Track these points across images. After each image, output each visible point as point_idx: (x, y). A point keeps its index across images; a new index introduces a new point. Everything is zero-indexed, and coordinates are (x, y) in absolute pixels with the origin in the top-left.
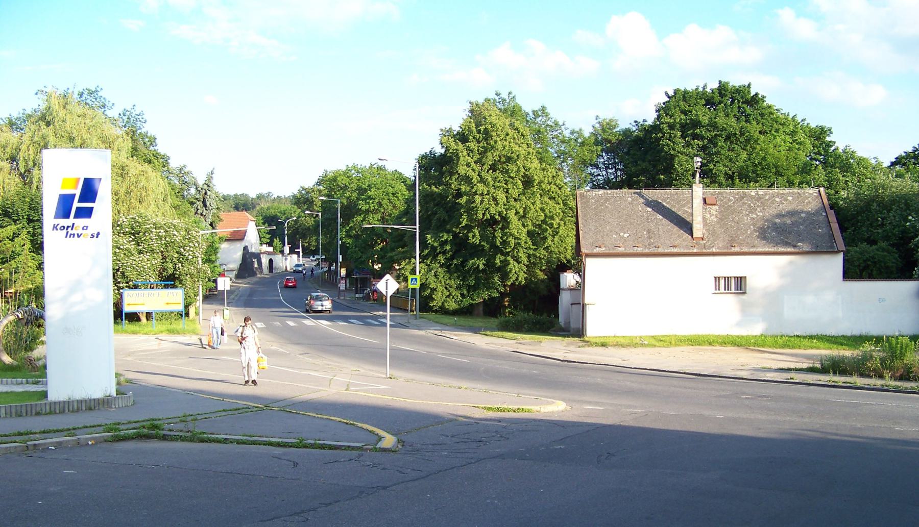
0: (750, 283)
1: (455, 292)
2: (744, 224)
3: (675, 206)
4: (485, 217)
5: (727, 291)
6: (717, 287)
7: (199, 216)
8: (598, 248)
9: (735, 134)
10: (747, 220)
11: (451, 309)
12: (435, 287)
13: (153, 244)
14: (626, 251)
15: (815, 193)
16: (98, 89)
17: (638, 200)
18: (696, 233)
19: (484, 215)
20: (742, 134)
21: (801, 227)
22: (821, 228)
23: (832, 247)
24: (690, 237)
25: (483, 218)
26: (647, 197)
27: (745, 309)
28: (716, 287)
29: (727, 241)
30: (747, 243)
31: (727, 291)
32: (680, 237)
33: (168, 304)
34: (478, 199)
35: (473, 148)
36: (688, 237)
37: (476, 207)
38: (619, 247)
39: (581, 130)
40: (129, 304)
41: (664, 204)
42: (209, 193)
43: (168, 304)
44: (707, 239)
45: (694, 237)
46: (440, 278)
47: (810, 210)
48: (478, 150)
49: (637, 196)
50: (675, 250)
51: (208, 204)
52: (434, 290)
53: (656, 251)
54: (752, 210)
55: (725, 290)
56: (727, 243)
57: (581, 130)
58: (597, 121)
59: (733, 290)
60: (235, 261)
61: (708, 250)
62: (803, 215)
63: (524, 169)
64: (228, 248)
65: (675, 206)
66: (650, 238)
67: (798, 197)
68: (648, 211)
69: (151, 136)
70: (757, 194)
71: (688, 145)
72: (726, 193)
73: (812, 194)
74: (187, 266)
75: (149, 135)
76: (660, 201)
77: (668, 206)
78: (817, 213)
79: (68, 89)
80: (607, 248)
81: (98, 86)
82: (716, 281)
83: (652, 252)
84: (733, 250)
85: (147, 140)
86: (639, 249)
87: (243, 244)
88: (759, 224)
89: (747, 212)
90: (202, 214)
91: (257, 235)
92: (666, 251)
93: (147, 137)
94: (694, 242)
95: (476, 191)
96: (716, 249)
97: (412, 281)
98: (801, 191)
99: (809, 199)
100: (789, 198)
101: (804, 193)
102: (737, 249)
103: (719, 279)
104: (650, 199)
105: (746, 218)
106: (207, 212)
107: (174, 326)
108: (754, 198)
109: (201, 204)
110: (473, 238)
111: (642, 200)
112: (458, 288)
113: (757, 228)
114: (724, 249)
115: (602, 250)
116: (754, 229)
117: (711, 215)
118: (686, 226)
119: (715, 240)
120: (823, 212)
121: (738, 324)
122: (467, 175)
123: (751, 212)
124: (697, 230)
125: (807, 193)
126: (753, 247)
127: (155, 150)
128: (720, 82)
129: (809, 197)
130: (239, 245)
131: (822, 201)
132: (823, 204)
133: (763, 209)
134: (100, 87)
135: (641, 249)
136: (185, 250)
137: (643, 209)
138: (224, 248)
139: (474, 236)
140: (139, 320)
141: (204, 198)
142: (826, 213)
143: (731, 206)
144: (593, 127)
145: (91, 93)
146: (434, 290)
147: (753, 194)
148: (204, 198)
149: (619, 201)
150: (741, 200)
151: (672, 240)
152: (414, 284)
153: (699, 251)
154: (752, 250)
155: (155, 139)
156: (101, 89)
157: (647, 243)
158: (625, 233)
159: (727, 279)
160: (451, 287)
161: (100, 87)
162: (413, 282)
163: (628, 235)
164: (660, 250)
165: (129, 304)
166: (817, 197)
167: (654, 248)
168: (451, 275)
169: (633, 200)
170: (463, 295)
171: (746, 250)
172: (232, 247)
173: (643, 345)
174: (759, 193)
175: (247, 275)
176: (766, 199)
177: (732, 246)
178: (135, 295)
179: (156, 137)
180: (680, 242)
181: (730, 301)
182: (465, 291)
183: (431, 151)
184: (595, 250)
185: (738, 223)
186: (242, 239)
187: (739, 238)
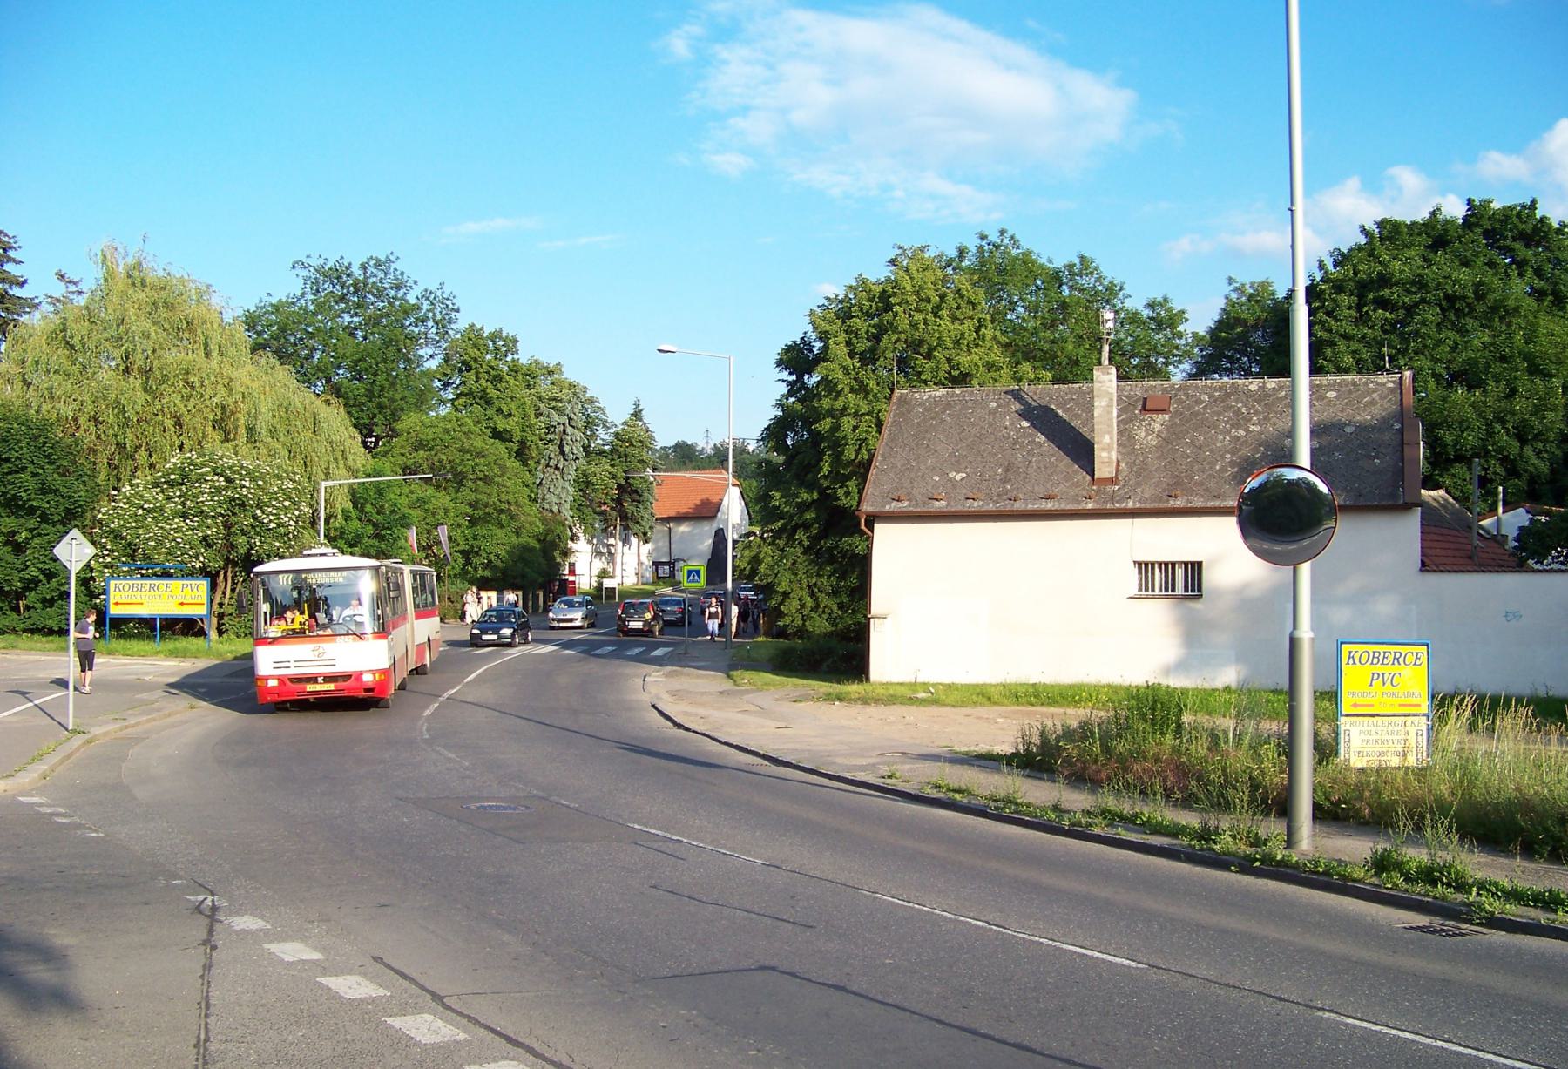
0: (1210, 578)
1: (825, 601)
2: (1212, 451)
3: (1081, 415)
4: (860, 456)
5: (1143, 593)
6: (1146, 585)
7: (552, 470)
8: (894, 504)
9: (1464, 298)
10: (1223, 441)
11: (818, 632)
12: (788, 590)
13: (202, 502)
14: (949, 509)
15: (1391, 382)
16: (392, 258)
17: (1008, 405)
18: (1100, 469)
19: (858, 451)
20: (1480, 297)
21: (1337, 454)
22: (1381, 455)
23: (1394, 496)
24: (1089, 478)
25: (856, 457)
26: (1030, 400)
27: (1193, 634)
28: (1140, 585)
29: (1164, 486)
30: (1207, 490)
31: (1143, 593)
32: (1068, 477)
33: (182, 604)
34: (847, 423)
35: (857, 329)
36: (1084, 478)
37: (844, 438)
38: (937, 500)
39: (1165, 299)
40: (117, 604)
41: (1060, 412)
42: (569, 430)
43: (182, 604)
44: (1122, 483)
45: (1096, 477)
46: (800, 575)
47: (1369, 418)
48: (867, 333)
49: (1010, 397)
50: (1049, 505)
51: (566, 449)
52: (786, 595)
53: (1009, 508)
54: (1240, 421)
55: (1186, 590)
56: (1164, 490)
57: (1165, 299)
58: (1231, 288)
59: (1180, 590)
60: (699, 556)
61: (1117, 505)
62: (1348, 430)
63: (949, 363)
64: (689, 532)
65: (1081, 415)
66: (1004, 481)
67: (1350, 392)
68: (1022, 428)
69: (507, 337)
70: (1263, 388)
71: (1363, 319)
72: (1197, 387)
73: (1384, 384)
74: (269, 540)
75: (504, 335)
76: (1053, 407)
77: (1065, 416)
78: (1384, 424)
79: (342, 257)
80: (914, 502)
81: (392, 253)
82: (1140, 572)
83: (1002, 509)
84: (1172, 503)
85: (501, 343)
86: (976, 504)
87: (715, 526)
88: (1246, 451)
89: (1228, 426)
90: (557, 468)
91: (742, 511)
92: (1030, 507)
93: (501, 338)
94: (1095, 487)
95: (845, 409)
96: (1134, 502)
97: (689, 577)
98: (1360, 379)
99: (1374, 395)
100: (1331, 395)
101: (1366, 384)
102: (1179, 503)
103: (1153, 568)
104: (1034, 404)
105: (1221, 438)
106: (567, 463)
107: (110, 646)
108: (1254, 395)
109: (557, 449)
110: (846, 497)
111: (1017, 406)
112: (835, 593)
113: (1240, 457)
114: (1152, 502)
115: (904, 506)
116: (1232, 460)
117: (1149, 431)
118: (1080, 450)
119: (1138, 484)
120: (1396, 421)
121: (1181, 666)
122: (830, 378)
123: (1237, 426)
124: (1103, 463)
125: (1372, 382)
126: (1216, 497)
127: (513, 360)
128: (1469, 202)
129: (1374, 392)
130: (707, 528)
131: (1401, 400)
132: (1402, 404)
133: (1265, 418)
134: (395, 255)
135: (981, 503)
136: (263, 513)
137: (1011, 424)
138: (683, 533)
139: (847, 494)
140: (202, 633)
141: (562, 440)
142: (1402, 424)
143: (1198, 413)
144: (1227, 298)
145: (378, 264)
146: (786, 595)
147: (1253, 387)
148: (562, 440)
149: (971, 408)
150: (1223, 401)
151: (1049, 486)
152: (693, 581)
153: (1098, 507)
154: (1216, 503)
155: (515, 341)
156: (398, 258)
157: (996, 490)
158: (958, 472)
159: (1168, 567)
160: (821, 591)
161: (395, 255)
162: (691, 578)
163: (964, 475)
164: (1018, 506)
165: (117, 604)
166: (1392, 391)
167: (1007, 502)
168: (821, 568)
169: (999, 406)
170: (841, 606)
171: (1198, 503)
172: (696, 531)
173: (912, 701)
174: (1269, 386)
175: (718, 580)
176: (1278, 398)
177: (1170, 496)
178: (127, 588)
179: (518, 338)
180: (1065, 489)
181: (1158, 615)
182: (846, 600)
183: (802, 339)
184: (888, 507)
185: (1200, 448)
186: (713, 517)
187: (1192, 478)
